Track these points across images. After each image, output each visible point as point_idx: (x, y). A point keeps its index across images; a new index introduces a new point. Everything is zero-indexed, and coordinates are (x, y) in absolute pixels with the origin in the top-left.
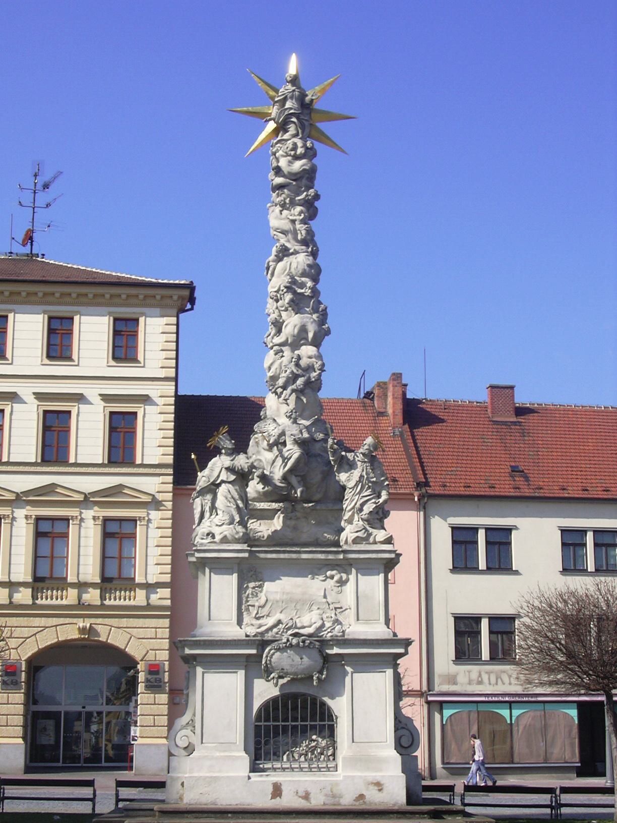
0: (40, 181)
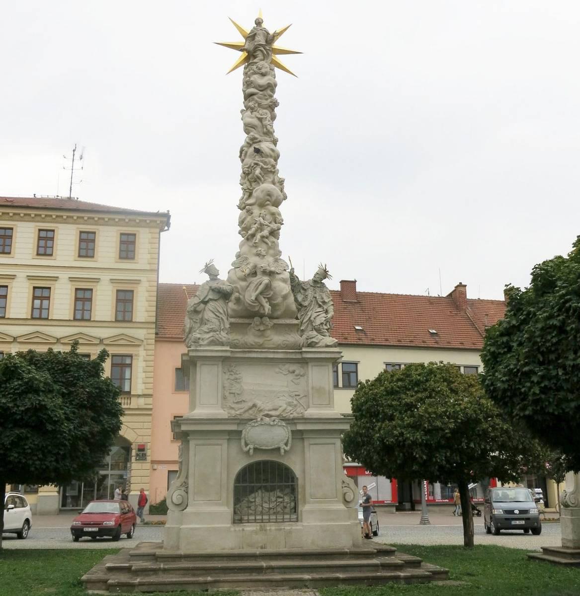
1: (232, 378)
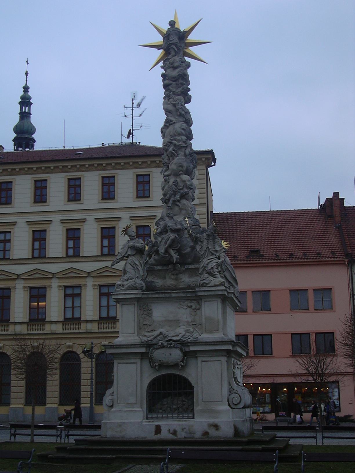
0: (136, 102)
1: (145, 313)
